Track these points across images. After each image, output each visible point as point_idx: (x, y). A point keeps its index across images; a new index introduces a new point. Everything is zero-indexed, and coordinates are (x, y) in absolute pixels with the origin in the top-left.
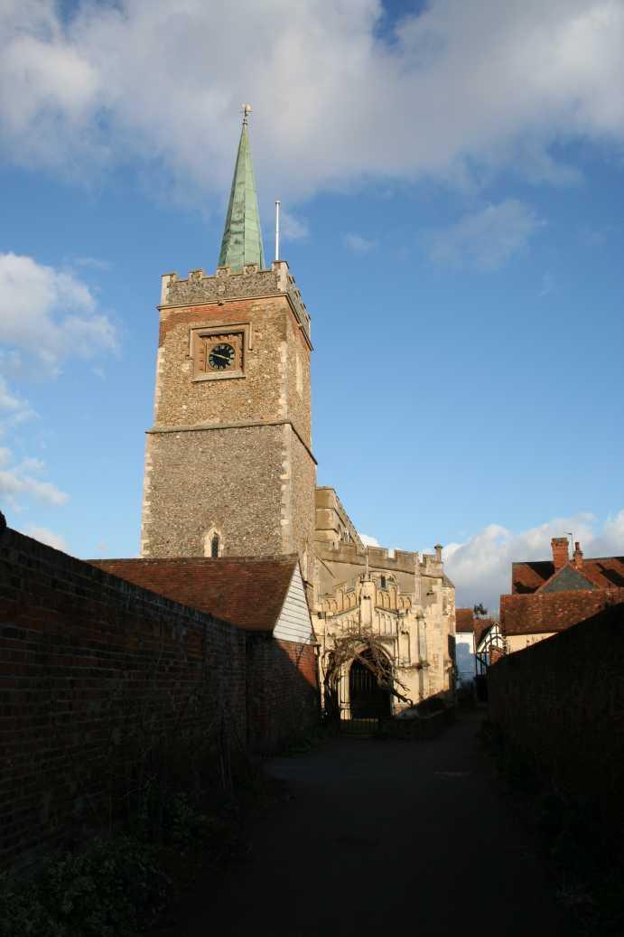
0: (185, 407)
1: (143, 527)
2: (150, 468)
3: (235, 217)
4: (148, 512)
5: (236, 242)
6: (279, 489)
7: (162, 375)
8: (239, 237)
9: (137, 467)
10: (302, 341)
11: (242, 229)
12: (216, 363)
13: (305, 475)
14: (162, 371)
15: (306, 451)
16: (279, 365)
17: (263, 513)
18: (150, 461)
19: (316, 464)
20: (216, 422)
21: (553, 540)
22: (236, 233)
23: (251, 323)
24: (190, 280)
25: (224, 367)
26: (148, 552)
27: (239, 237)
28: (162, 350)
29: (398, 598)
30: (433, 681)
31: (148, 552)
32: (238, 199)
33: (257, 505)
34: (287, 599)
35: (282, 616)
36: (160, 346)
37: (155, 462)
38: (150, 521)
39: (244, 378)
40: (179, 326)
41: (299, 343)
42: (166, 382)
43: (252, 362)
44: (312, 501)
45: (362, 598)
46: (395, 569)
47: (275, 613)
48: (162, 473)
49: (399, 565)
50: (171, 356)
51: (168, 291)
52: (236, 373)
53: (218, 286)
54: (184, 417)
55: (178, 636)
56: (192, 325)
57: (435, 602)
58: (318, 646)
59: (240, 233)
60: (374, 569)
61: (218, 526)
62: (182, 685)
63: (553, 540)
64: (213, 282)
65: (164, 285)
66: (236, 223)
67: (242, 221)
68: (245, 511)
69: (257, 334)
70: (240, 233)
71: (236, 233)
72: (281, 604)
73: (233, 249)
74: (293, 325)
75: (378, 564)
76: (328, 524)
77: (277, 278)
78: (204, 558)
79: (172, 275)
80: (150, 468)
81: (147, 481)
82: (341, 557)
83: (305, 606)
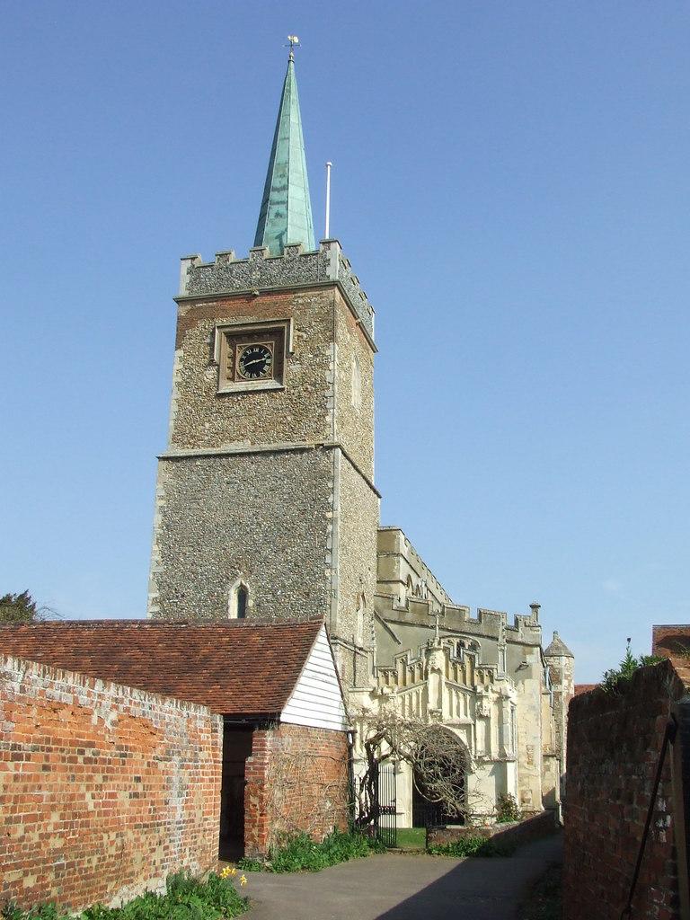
0: (207, 425)
1: (151, 576)
2: (162, 503)
3: (276, 182)
4: (158, 558)
5: (278, 215)
6: (324, 530)
7: (179, 384)
8: (281, 209)
9: (144, 499)
10: (361, 341)
11: (284, 198)
12: (251, 373)
13: (360, 513)
14: (180, 380)
15: (364, 482)
16: (327, 373)
17: (303, 561)
18: (163, 493)
19: (380, 497)
20: (245, 446)
21: (23, 599)
22: (278, 203)
23: (292, 320)
24: (216, 264)
25: (258, 375)
26: (156, 609)
27: (281, 209)
28: (180, 353)
29: (476, 672)
30: (526, 780)
31: (156, 609)
32: (279, 158)
33: (295, 551)
34: (305, 673)
35: (295, 694)
36: (178, 347)
37: (169, 494)
38: (161, 569)
39: (282, 390)
40: (201, 324)
41: (356, 343)
42: (184, 394)
43: (292, 369)
44: (372, 545)
45: (430, 669)
46: (475, 642)
47: (284, 690)
48: (176, 509)
49: (483, 629)
50: (191, 360)
51: (187, 278)
52: (271, 384)
53: (251, 272)
54: (206, 438)
55: (101, 720)
56: (219, 322)
57: (530, 677)
58: (353, 733)
59: (283, 202)
60: (449, 634)
61: (245, 577)
62: (105, 778)
63: (23, 599)
64: (245, 267)
65: (184, 271)
66: (278, 190)
67: (285, 188)
68: (281, 556)
69: (300, 333)
70: (283, 202)
71: (278, 203)
72: (294, 680)
73: (274, 225)
74: (347, 320)
75: (454, 626)
76: (394, 574)
77: (327, 262)
78: (229, 621)
79: (193, 259)
80: (162, 503)
81: (158, 518)
82: (409, 617)
83: (336, 682)
